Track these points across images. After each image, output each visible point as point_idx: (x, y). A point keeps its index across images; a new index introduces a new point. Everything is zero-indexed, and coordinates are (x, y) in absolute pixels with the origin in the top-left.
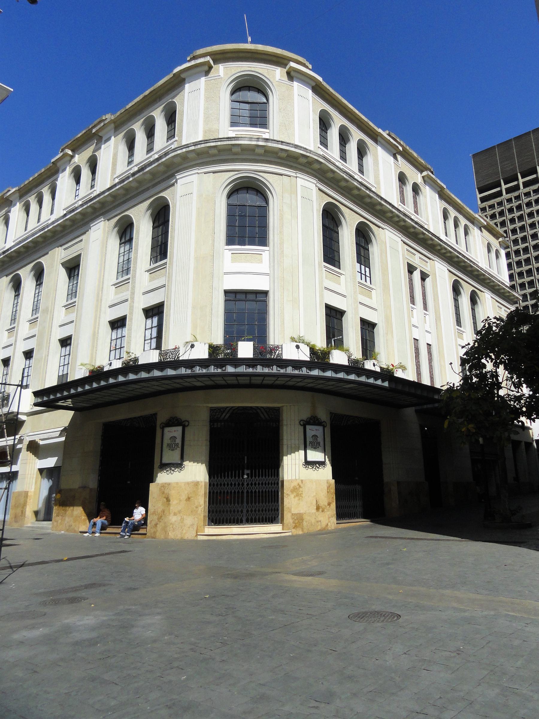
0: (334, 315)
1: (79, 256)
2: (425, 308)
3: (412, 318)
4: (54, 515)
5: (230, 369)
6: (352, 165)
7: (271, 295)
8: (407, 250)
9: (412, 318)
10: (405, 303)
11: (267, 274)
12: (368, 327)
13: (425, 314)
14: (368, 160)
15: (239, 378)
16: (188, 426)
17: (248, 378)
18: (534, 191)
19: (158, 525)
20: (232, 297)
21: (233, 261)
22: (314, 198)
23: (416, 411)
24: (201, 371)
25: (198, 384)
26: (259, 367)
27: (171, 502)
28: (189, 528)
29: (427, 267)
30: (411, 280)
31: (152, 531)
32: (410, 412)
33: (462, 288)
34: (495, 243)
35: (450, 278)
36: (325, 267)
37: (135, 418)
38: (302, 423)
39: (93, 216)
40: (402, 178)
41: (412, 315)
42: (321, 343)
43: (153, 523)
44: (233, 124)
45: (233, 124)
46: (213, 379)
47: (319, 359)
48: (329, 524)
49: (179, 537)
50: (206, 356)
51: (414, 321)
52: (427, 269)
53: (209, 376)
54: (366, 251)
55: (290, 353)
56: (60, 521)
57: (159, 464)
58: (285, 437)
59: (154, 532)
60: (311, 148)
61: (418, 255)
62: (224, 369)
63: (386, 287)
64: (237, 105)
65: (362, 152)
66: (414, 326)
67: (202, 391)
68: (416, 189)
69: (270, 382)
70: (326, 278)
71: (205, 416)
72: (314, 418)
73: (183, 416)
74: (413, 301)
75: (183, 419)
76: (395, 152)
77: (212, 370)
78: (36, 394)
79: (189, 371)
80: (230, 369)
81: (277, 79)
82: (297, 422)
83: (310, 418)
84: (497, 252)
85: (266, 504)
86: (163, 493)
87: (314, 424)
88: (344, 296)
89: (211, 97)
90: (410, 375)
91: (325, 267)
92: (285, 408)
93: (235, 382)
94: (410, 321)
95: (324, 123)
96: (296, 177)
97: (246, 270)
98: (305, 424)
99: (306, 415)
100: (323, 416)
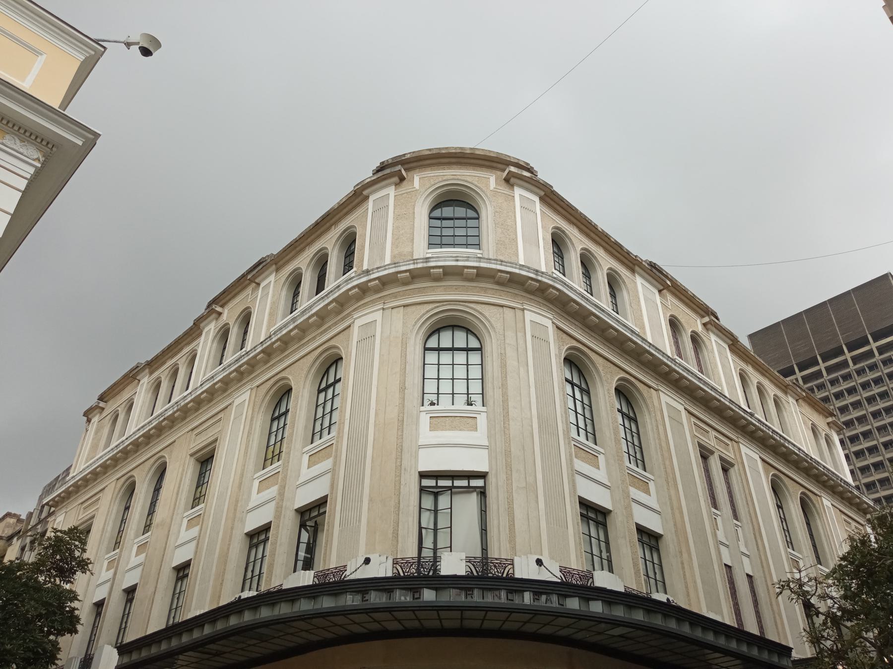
0: (594, 515)
5: (428, 595)
6: (602, 300)
13: (737, 526)
14: (624, 296)
15: (443, 614)
18: (886, 445)
21: (433, 428)
22: (552, 340)
24: (378, 601)
29: (729, 451)
30: (707, 471)
34: (821, 423)
35: (766, 472)
40: (674, 324)
44: (431, 245)
45: (431, 245)
46: (398, 615)
52: (730, 455)
61: (713, 433)
64: (438, 223)
65: (613, 283)
68: (695, 339)
69: (496, 625)
70: (576, 457)
76: (662, 288)
80: (428, 595)
81: (492, 188)
84: (828, 440)
89: (405, 216)
93: (436, 624)
94: (715, 535)
95: (558, 243)
96: (523, 310)
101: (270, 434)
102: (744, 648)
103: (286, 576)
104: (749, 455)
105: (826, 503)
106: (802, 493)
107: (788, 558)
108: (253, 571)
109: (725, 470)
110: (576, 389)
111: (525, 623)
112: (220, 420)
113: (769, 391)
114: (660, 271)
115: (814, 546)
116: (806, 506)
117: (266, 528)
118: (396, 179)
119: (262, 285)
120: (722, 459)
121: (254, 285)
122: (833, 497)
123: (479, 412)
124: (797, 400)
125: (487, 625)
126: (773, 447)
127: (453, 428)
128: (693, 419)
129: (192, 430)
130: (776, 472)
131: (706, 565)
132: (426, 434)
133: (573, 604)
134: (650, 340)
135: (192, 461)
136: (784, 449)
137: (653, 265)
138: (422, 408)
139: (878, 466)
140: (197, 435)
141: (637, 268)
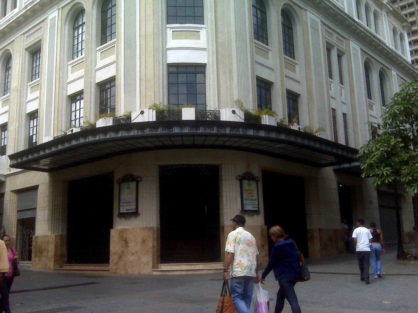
0: (264, 88)
1: (40, 41)
2: (341, 82)
3: (330, 91)
4: (33, 256)
7: (207, 65)
8: (326, 30)
9: (330, 91)
10: (324, 76)
11: (204, 49)
12: (293, 98)
15: (184, 138)
16: (141, 181)
17: (192, 138)
19: (119, 263)
20: (174, 70)
23: (335, 171)
25: (149, 145)
27: (129, 245)
28: (145, 265)
29: (343, 46)
31: (114, 268)
32: (329, 172)
33: (372, 64)
35: (362, 56)
36: (255, 43)
38: (238, 178)
41: (330, 87)
42: (252, 107)
43: (115, 261)
47: (252, 121)
48: (263, 262)
49: (136, 273)
51: (332, 93)
52: (343, 47)
53: (158, 137)
56: (37, 261)
57: (118, 213)
58: (225, 211)
59: (116, 269)
61: (335, 35)
63: (307, 63)
66: (332, 97)
73: (136, 173)
74: (331, 75)
77: (160, 131)
78: (12, 157)
79: (140, 133)
80: (176, 130)
85: (208, 245)
86: (122, 237)
88: (272, 70)
90: (328, 136)
91: (255, 43)
93: (181, 143)
94: (328, 93)
97: (187, 47)
98: (241, 179)
99: (241, 171)
100: (257, 173)
101: (74, 37)
103: (96, 119)
104: (354, 48)
105: (394, 73)
106: (381, 68)
107: (366, 104)
108: (75, 116)
109: (339, 57)
110: (258, 11)
111: (226, 142)
112: (41, 28)
113: (372, 7)
116: (382, 77)
117: (80, 93)
120: (338, 50)
122: (398, 70)
123: (201, 28)
124: (387, 13)
125: (206, 143)
126: (370, 43)
127: (186, 38)
128: (325, 27)
129: (24, 34)
130: (368, 57)
132: (171, 43)
133: (251, 132)
135: (27, 54)
136: (363, 34)
138: (168, 26)
140: (27, 37)
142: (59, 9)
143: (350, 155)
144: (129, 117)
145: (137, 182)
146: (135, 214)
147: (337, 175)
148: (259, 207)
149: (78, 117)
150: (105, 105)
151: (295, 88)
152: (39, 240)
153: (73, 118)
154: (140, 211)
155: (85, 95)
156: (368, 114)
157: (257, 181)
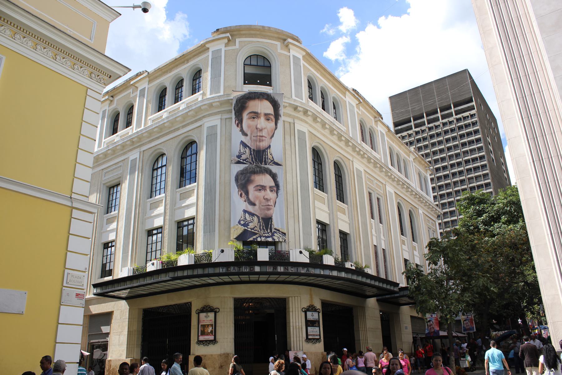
0: (323, 227)
23: (378, 300)
24: (234, 271)
26: (343, 273)
32: (372, 302)
35: (396, 199)
37: (171, 305)
39: (131, 148)
50: (232, 259)
54: (337, 173)
55: (295, 257)
60: (304, 101)
62: (252, 269)
67: (329, 291)
71: (230, 305)
72: (312, 306)
73: (215, 304)
75: (215, 307)
82: (300, 310)
83: (309, 307)
87: (207, 311)
92: (290, 299)
93: (239, 279)
99: (306, 305)
100: (318, 306)
101: (152, 178)
102: (381, 285)
114: (357, 93)
115: (411, 222)
118: (226, 41)
119: (139, 89)
121: (419, 268)
128: (367, 175)
131: (367, 247)
134: (351, 136)
137: (354, 90)
139: (450, 203)
141: (347, 93)
142: (221, 119)
143: (392, 288)
144: (209, 255)
145: (216, 313)
146: (214, 341)
147: (379, 304)
148: (320, 335)
149: (154, 249)
150: (185, 240)
151: (346, 230)
152: (113, 364)
153: (149, 250)
154: (217, 339)
155: (166, 232)
156: (402, 249)
157: (319, 312)
